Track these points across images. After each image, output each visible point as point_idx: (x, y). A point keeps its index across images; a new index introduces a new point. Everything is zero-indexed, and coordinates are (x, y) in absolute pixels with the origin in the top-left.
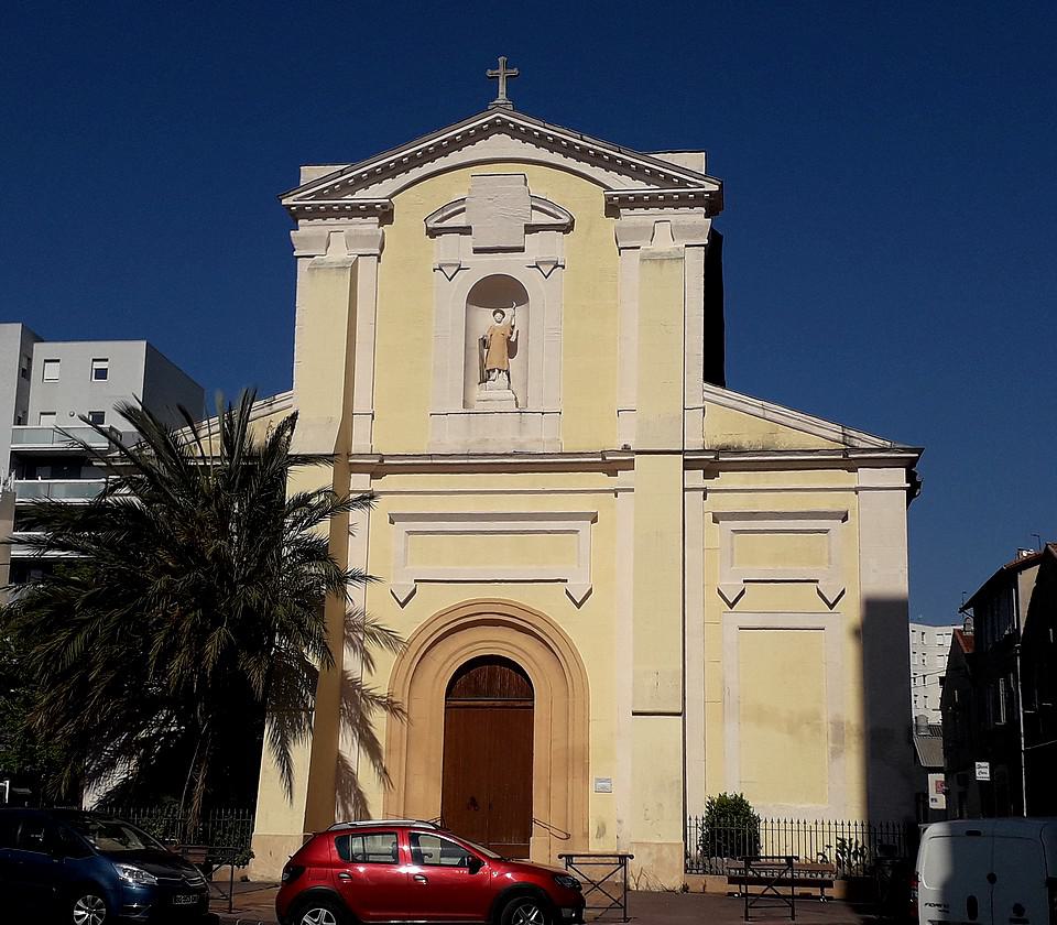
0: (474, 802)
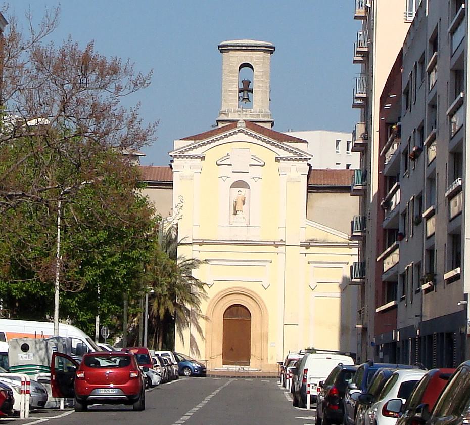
0: (232, 349)
